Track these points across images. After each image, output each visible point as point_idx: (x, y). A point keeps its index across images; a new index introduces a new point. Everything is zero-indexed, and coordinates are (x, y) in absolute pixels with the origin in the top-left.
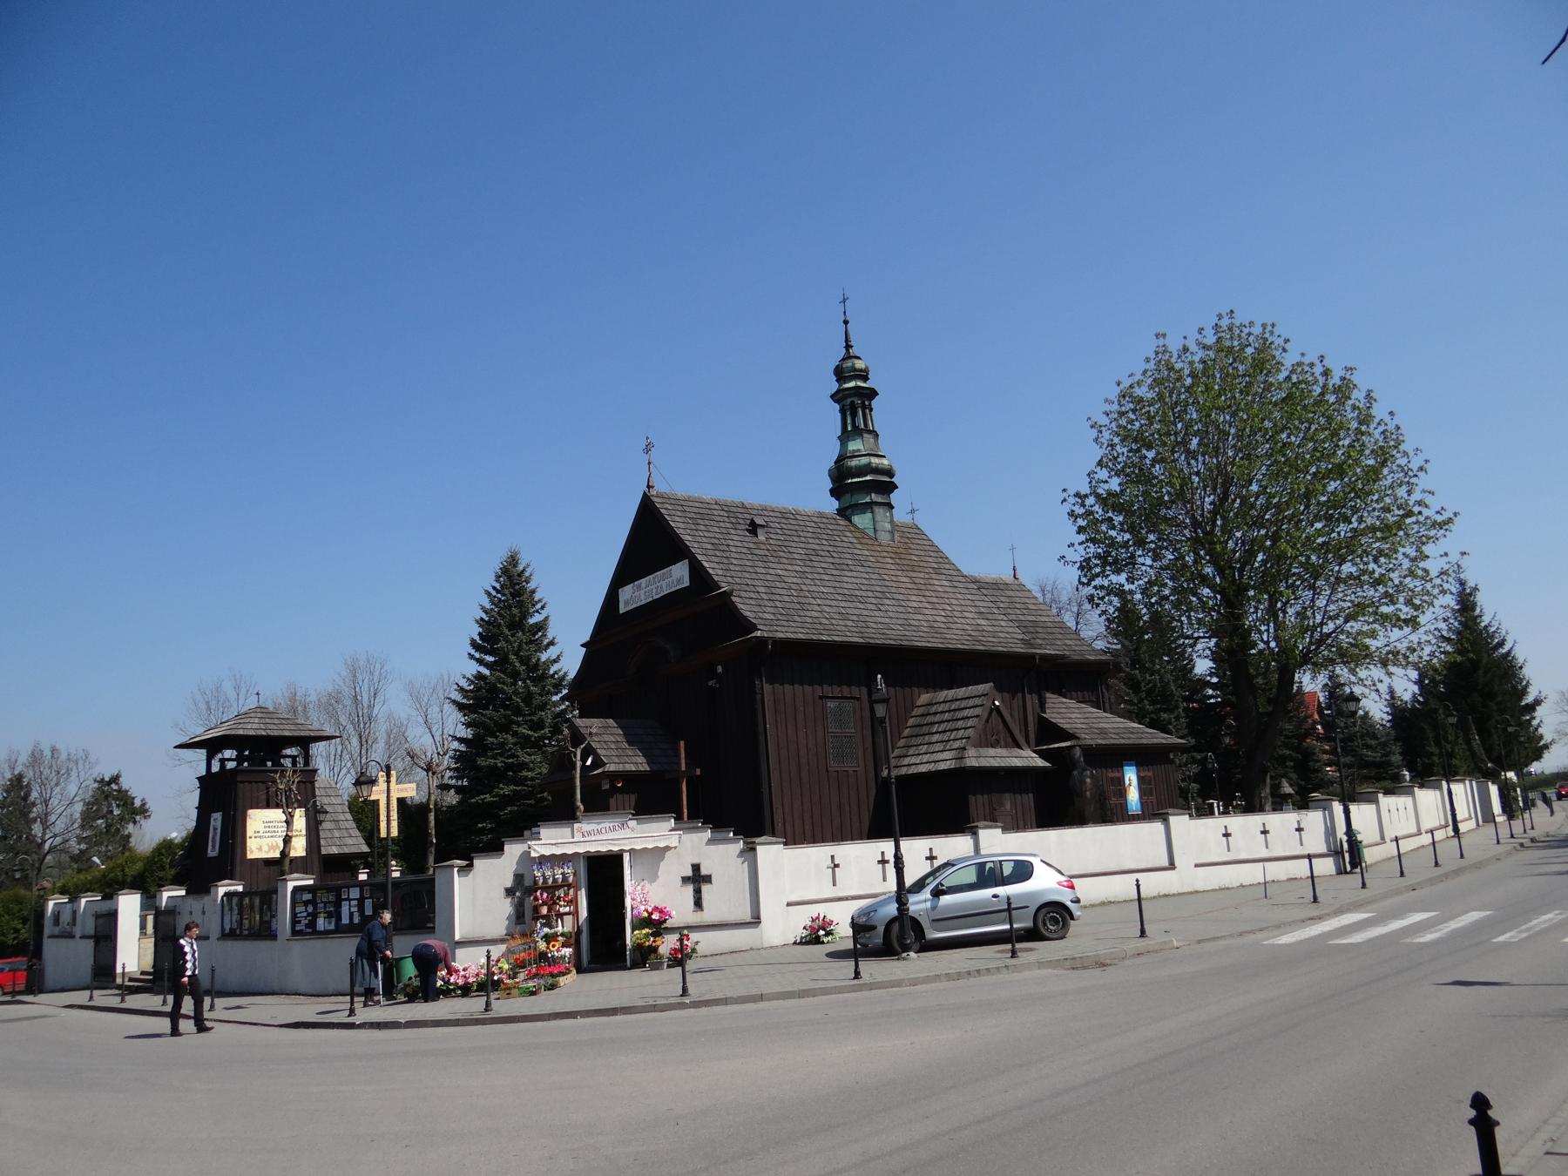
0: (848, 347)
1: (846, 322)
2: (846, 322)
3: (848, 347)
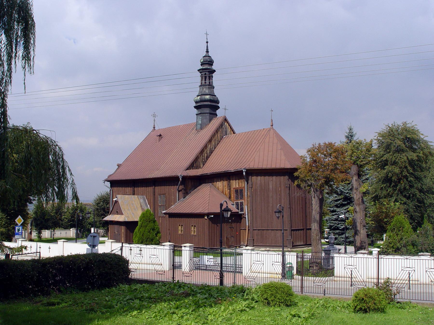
0: (207, 52)
1: (207, 42)
2: (207, 42)
3: (207, 52)
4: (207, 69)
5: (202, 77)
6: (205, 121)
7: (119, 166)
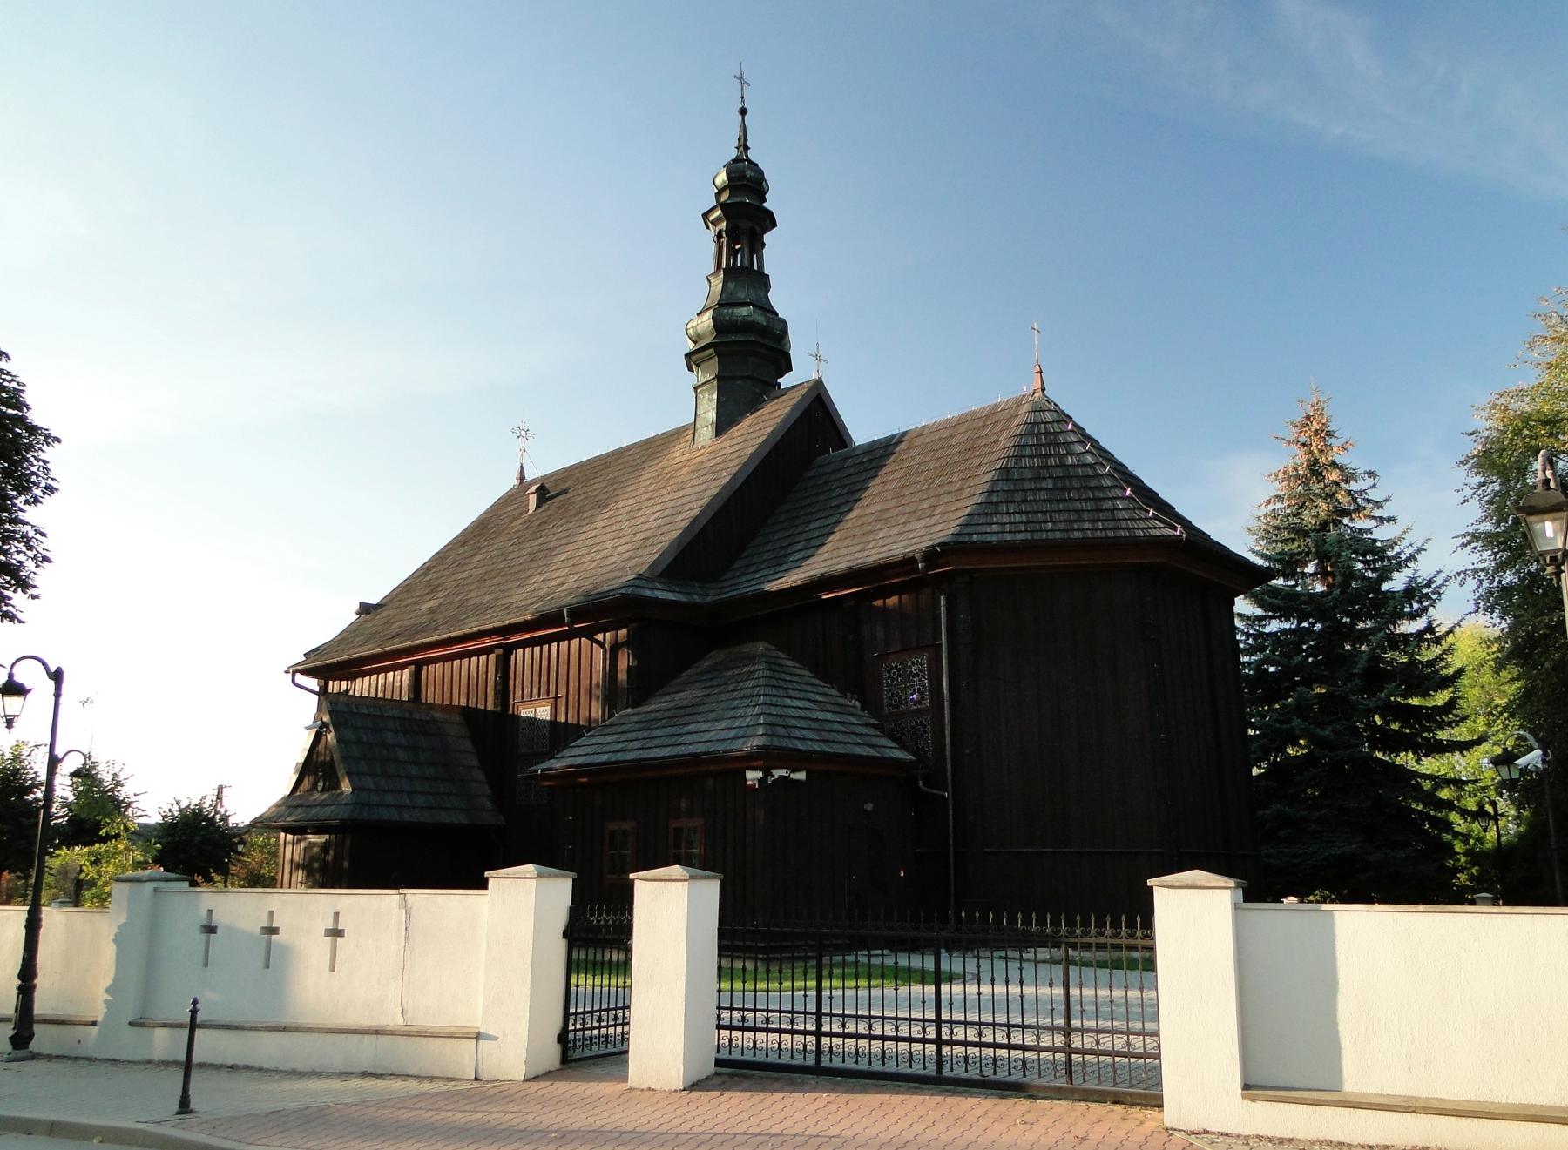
1: (743, 112)
2: (743, 112)
7: (365, 609)
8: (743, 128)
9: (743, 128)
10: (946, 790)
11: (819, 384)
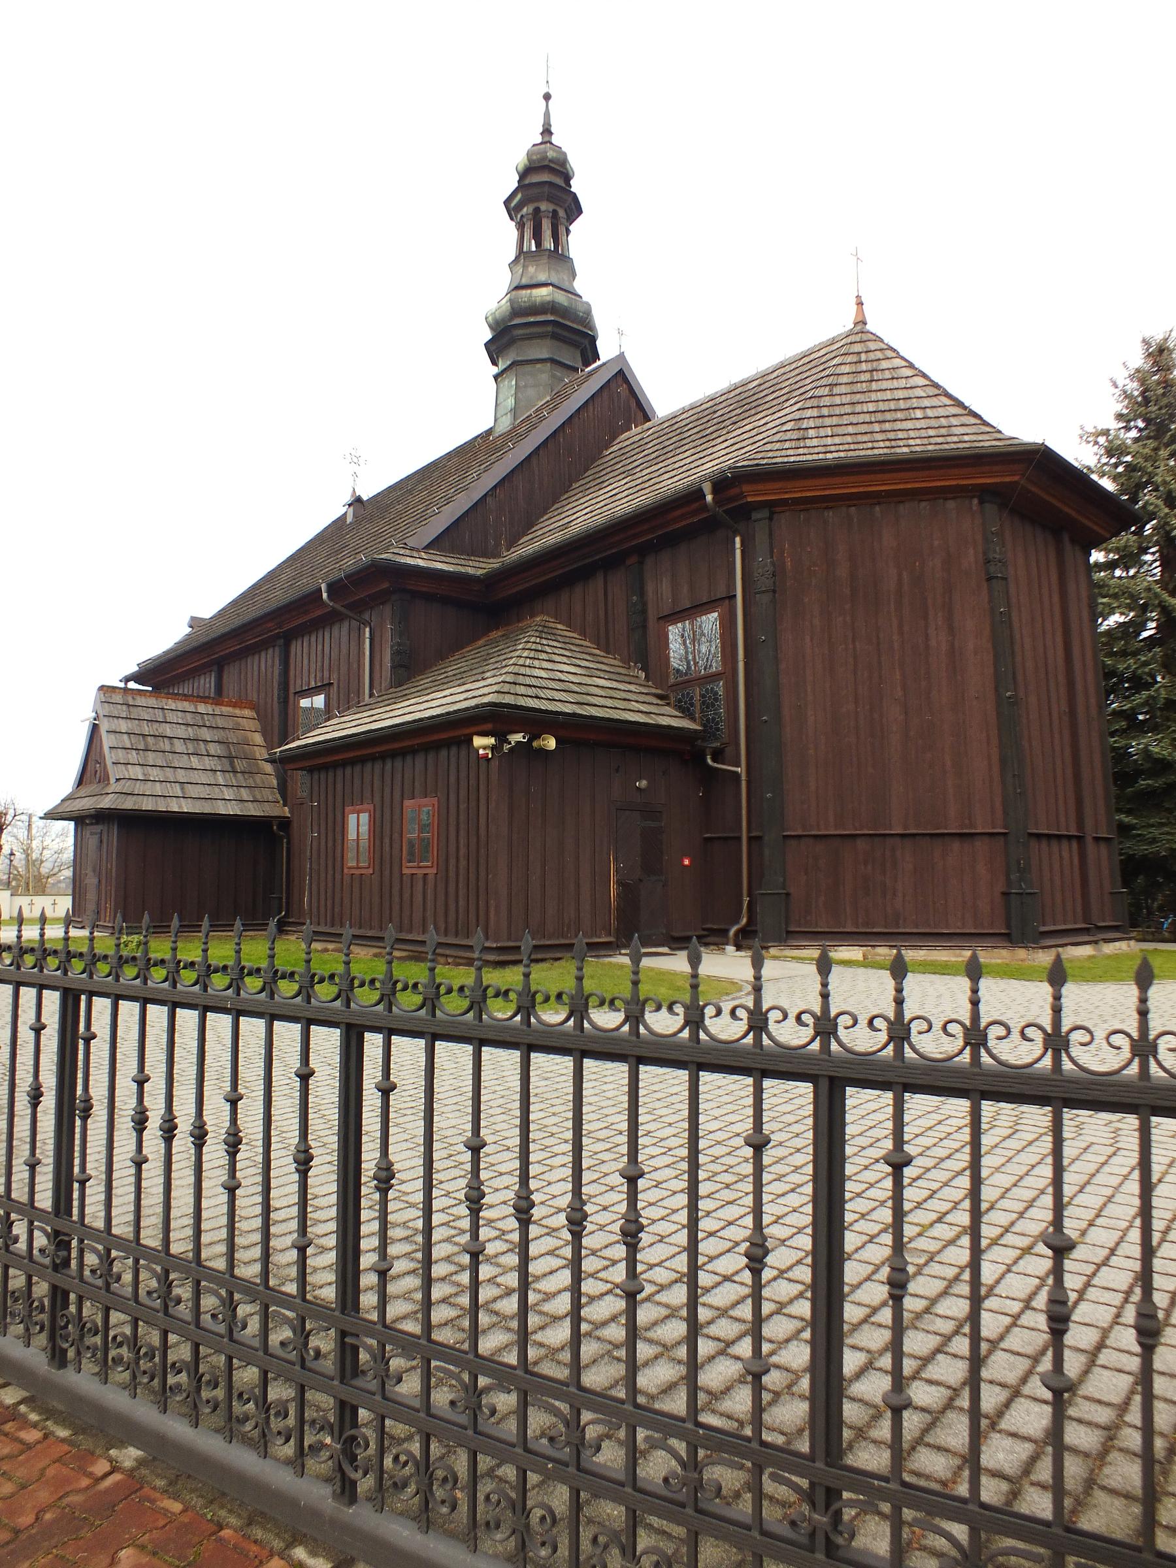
0: (547, 131)
1: (547, 97)
2: (547, 97)
3: (547, 131)
4: (545, 197)
5: (521, 227)
6: (531, 392)
8: (547, 115)
9: (547, 115)
10: (738, 765)
11: (621, 357)
